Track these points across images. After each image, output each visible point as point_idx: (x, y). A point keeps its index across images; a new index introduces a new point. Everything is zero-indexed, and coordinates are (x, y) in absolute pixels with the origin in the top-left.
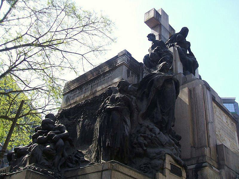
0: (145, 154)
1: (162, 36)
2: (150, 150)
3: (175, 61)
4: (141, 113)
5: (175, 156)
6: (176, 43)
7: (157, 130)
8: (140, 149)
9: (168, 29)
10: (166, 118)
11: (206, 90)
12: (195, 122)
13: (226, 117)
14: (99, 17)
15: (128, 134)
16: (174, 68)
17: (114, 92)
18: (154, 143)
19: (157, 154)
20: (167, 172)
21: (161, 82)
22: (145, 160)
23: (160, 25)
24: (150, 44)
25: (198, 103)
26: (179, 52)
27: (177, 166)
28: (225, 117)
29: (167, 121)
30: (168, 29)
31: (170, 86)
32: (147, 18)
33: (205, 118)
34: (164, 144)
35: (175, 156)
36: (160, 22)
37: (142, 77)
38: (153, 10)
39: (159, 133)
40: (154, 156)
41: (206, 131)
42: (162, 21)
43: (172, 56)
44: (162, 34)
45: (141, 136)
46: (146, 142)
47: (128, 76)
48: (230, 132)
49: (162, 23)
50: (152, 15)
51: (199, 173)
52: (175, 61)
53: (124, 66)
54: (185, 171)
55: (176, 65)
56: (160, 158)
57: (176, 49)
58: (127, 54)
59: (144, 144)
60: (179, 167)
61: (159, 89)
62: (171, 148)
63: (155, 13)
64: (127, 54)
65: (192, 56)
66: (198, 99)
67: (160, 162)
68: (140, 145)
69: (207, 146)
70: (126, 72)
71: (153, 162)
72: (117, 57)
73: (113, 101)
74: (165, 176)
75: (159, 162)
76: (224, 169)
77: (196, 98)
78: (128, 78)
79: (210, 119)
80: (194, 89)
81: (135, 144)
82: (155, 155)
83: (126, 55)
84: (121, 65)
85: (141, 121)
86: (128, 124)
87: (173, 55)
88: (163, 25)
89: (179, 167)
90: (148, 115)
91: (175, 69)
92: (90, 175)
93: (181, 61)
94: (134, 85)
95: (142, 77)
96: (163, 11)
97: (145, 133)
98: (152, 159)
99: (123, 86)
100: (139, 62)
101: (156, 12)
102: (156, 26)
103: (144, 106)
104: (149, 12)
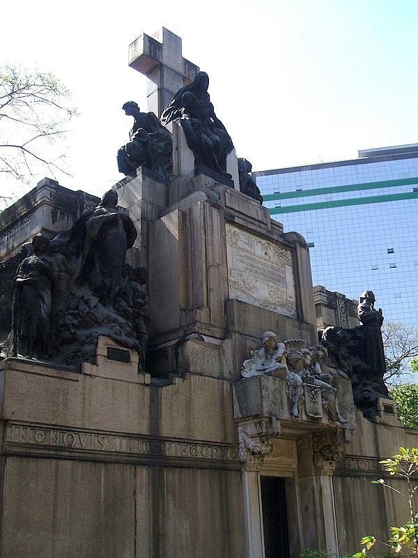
0: (74, 339)
1: (164, 91)
2: (82, 333)
3: (177, 149)
4: (75, 277)
5: (115, 336)
6: (184, 109)
7: (94, 301)
8: (68, 332)
9: (181, 70)
10: (107, 282)
11: (211, 211)
12: (190, 268)
13: (263, 245)
14: (35, 76)
15: (45, 317)
16: (174, 165)
17: (30, 251)
18: (89, 321)
19: (88, 337)
20: (100, 360)
21: (97, 227)
22: (74, 347)
23: (156, 67)
24: (131, 120)
25: (195, 233)
26: (184, 130)
27: (121, 348)
28: (260, 246)
29: (108, 286)
30: (181, 70)
31: (113, 231)
32: (131, 58)
33: (204, 259)
34: (101, 320)
35: (115, 336)
36: (158, 61)
37: (81, 212)
38: (143, 36)
39: (95, 306)
40: (84, 341)
41: (205, 283)
42: (166, 58)
43: (171, 141)
44: (165, 87)
45: (69, 313)
46: (76, 322)
47: (54, 222)
48: (271, 270)
49: (165, 61)
50: (140, 49)
51: (179, 351)
52: (177, 149)
53: (45, 205)
54: (137, 353)
55: (179, 158)
56: (91, 343)
57: (180, 125)
58: (49, 184)
59: (72, 324)
60: (126, 349)
61: (96, 239)
62: (110, 326)
63: (148, 44)
64: (49, 184)
65: (222, 129)
66: (195, 227)
67: (91, 347)
68: (66, 326)
69: (205, 306)
70: (50, 215)
71: (83, 349)
72: (34, 191)
73: (27, 267)
74: (98, 365)
75: (88, 348)
76: (231, 338)
77: (193, 227)
78: (53, 224)
79: (215, 257)
80: (190, 210)
81: (62, 326)
82: (84, 339)
83: (48, 186)
84: (41, 204)
85: (75, 290)
86: (46, 301)
87: (174, 138)
88: (166, 66)
89: (126, 349)
90: (84, 279)
91: (176, 167)
92: (134, 430)
93: (190, 147)
94: (63, 234)
95: (81, 212)
96: (168, 34)
97: (77, 309)
98: (83, 344)
99: (40, 245)
100: (211, 101)
101: (150, 42)
102: (153, 70)
103: (77, 266)
104: (135, 42)
